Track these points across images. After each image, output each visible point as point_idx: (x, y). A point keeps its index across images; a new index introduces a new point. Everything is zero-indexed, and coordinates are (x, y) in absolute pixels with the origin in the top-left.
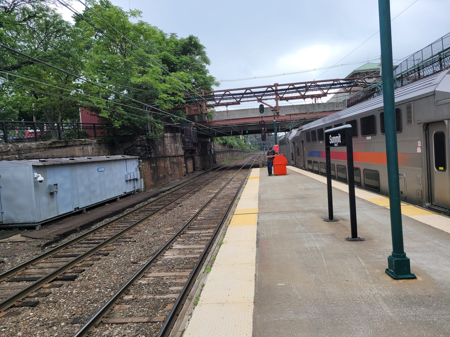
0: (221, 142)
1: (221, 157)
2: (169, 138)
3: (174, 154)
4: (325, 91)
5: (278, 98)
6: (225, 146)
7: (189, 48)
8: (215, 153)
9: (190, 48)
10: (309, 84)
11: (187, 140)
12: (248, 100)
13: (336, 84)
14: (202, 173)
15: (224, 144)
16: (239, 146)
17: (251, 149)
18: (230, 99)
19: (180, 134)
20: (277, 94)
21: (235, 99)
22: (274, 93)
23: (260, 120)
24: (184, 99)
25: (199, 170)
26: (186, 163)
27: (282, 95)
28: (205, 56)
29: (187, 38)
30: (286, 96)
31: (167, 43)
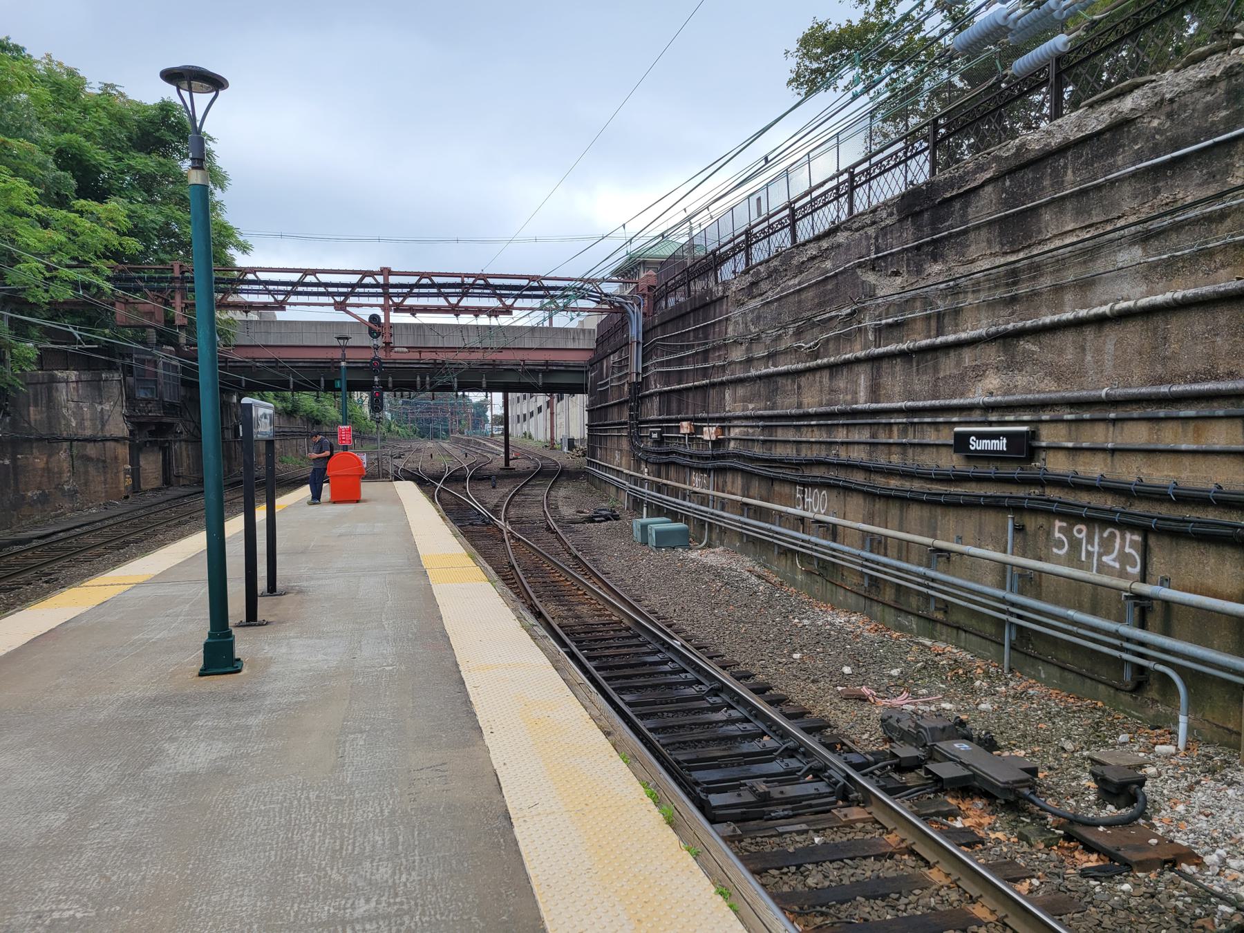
2: (73, 385)
3: (88, 433)
4: (509, 302)
5: (390, 306)
6: (292, 419)
10: (471, 280)
11: (141, 394)
17: (389, 431)
18: (258, 292)
19: (117, 376)
20: (387, 296)
22: (380, 290)
24: (108, 279)
26: (134, 461)
27: (401, 299)
28: (211, 162)
29: (141, 102)
30: (410, 301)
31: (85, 110)
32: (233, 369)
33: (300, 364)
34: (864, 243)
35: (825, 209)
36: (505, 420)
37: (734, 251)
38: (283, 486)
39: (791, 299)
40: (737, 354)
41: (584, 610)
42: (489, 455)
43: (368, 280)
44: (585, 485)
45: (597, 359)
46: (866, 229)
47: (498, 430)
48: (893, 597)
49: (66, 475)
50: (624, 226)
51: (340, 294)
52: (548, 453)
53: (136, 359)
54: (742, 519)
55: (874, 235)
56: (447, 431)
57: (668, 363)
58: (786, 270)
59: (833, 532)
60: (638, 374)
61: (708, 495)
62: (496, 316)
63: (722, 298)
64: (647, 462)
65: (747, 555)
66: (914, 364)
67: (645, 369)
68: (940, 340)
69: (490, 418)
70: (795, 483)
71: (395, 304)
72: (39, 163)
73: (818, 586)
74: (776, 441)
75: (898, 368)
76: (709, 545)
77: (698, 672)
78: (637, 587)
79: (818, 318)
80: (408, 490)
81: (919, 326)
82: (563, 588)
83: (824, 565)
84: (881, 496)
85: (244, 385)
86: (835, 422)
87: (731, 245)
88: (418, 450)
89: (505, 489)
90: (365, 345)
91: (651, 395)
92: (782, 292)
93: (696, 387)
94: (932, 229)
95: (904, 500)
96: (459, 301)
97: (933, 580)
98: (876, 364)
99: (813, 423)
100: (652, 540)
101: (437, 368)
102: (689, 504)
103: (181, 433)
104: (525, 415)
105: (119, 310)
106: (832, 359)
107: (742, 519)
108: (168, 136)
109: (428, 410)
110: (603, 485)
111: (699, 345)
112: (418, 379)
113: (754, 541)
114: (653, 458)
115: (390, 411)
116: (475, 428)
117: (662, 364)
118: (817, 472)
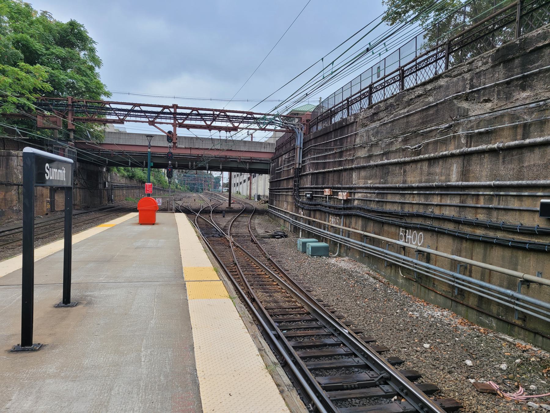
0: (126, 174)
1: (123, 193)
4: (236, 125)
5: (177, 124)
6: (132, 180)
7: (67, 38)
8: (113, 188)
9: (70, 38)
10: (218, 113)
12: (137, 120)
13: (250, 118)
14: (77, 213)
15: (131, 178)
16: (156, 183)
17: (177, 188)
20: (175, 119)
21: (118, 116)
22: (172, 116)
23: (167, 151)
24: (34, 103)
25: (79, 208)
26: (52, 197)
27: (182, 121)
30: (187, 122)
31: (32, 23)
32: (102, 155)
33: (134, 154)
34: (461, 83)
35: (427, 69)
36: (229, 185)
37: (342, 109)
38: (125, 211)
39: (401, 121)
40: (362, 153)
41: (278, 296)
42: (221, 201)
43: (166, 110)
44: (267, 218)
45: (275, 158)
46: (463, 75)
47: (225, 190)
48: (476, 303)
49: (15, 202)
50: (322, 59)
51: (151, 117)
52: (248, 201)
53: (54, 147)
54: (363, 244)
55: (469, 78)
56: (202, 189)
57: (318, 158)
58: (398, 105)
59: (428, 257)
60: (299, 164)
61: (339, 228)
62: (230, 132)
63: (353, 123)
64: (303, 209)
65: (364, 264)
66: (501, 158)
67: (303, 162)
68: (527, 141)
69: (221, 184)
70: (400, 226)
71: (179, 123)
72: (4, 45)
73: (414, 287)
74: (386, 202)
75: (485, 160)
76: (339, 256)
77: (367, 358)
78: (307, 281)
79: (422, 131)
80: (181, 218)
81: (506, 133)
82: (264, 280)
83: (420, 276)
84: (458, 237)
85: (107, 163)
86: (432, 192)
87: (359, 94)
88: (189, 197)
89: (229, 218)
90: (165, 146)
91: (307, 175)
92: (395, 117)
93: (335, 171)
94: (522, 69)
95: (488, 243)
96: (211, 123)
97: (518, 299)
98: (467, 158)
99: (415, 192)
100: (309, 251)
101: (199, 158)
102: (329, 233)
103: (77, 184)
104: (238, 183)
105: (39, 119)
106: (432, 155)
107: (363, 244)
108: (73, 40)
109: (194, 179)
110: (277, 218)
111: (336, 149)
112: (190, 163)
113: (369, 256)
114: (306, 207)
115: (178, 179)
116: (215, 188)
117: (314, 159)
118: (415, 221)
